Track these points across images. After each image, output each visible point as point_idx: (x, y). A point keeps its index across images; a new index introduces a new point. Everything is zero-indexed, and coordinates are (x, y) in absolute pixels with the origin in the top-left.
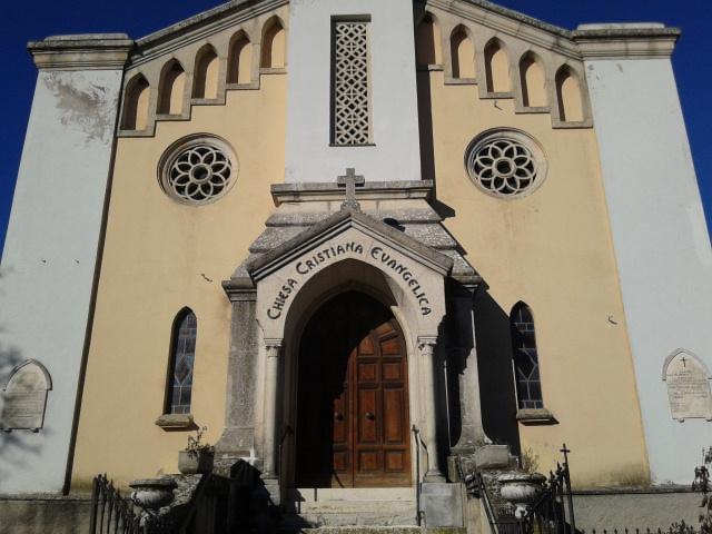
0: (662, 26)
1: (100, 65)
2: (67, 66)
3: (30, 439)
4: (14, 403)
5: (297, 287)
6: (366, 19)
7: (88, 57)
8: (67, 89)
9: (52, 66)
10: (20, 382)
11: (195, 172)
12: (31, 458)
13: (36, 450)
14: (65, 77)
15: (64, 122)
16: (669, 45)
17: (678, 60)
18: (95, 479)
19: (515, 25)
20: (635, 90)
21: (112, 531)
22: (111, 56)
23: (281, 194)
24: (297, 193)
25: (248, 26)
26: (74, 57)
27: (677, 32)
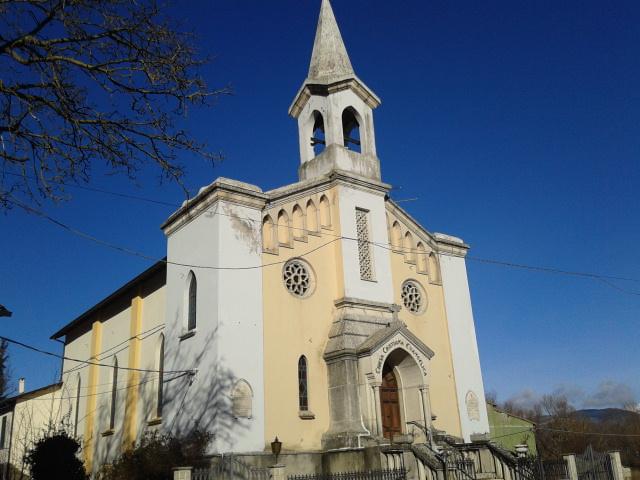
0: (462, 242)
1: (251, 205)
2: (234, 202)
3: (245, 421)
4: (236, 402)
5: (384, 359)
6: (367, 211)
7: (246, 199)
8: (235, 216)
9: (226, 199)
10: (238, 390)
11: (296, 279)
12: (246, 431)
13: (248, 427)
14: (232, 207)
15: (237, 238)
16: (464, 252)
17: (466, 258)
18: (272, 444)
19: (416, 228)
20: (455, 268)
21: (508, 477)
22: (257, 202)
23: (343, 303)
24: (353, 303)
25: (313, 197)
26: (239, 197)
27: (389, 186)
